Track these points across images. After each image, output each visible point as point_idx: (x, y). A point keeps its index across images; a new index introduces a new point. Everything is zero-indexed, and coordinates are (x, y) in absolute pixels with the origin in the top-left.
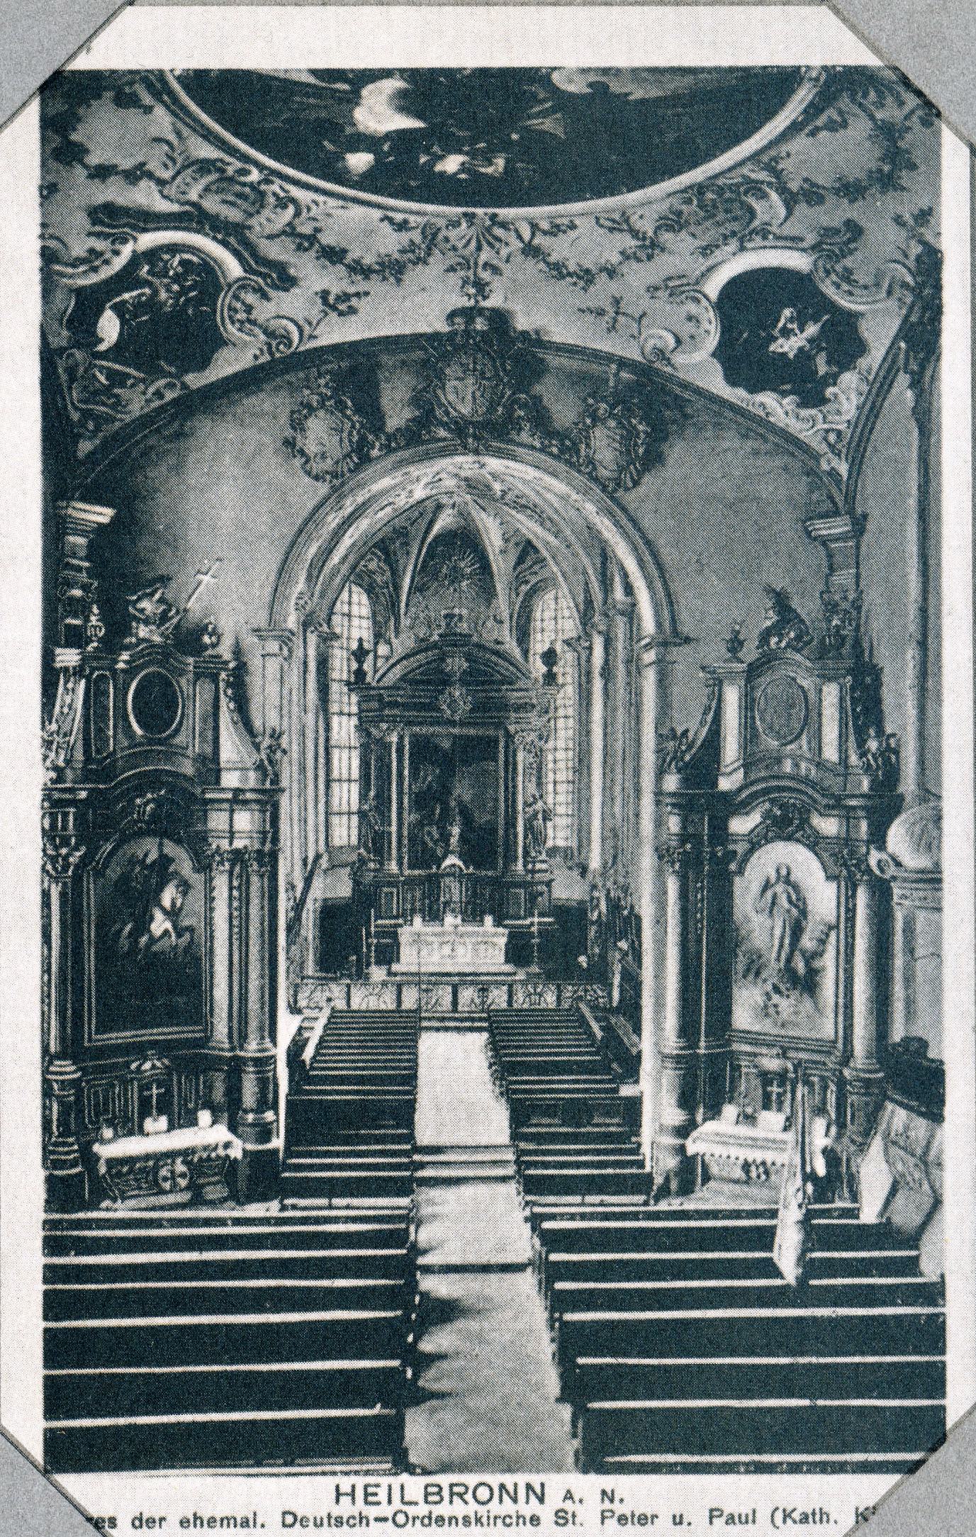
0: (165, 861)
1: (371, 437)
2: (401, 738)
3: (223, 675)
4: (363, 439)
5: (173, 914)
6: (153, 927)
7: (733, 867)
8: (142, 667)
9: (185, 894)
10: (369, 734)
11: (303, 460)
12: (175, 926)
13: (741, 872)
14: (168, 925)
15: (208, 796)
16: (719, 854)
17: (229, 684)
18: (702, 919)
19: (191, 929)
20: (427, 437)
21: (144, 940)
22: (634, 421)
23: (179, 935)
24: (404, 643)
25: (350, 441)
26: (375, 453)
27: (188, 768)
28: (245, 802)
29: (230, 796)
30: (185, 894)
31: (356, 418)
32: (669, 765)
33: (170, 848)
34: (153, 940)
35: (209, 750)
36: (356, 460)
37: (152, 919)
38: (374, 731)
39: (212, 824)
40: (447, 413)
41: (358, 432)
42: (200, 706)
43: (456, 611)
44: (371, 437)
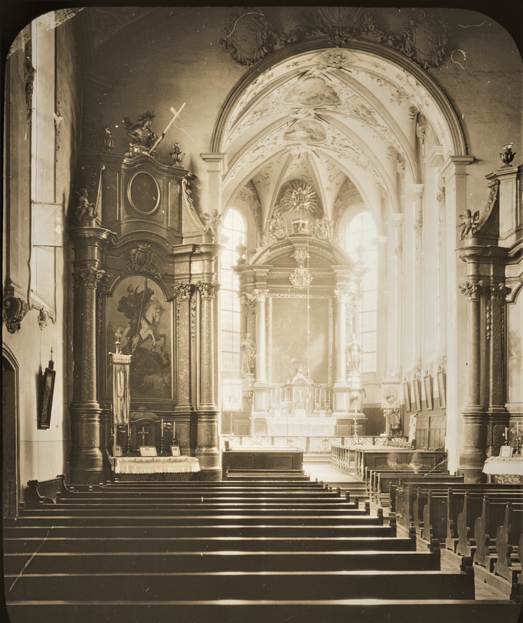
0: (149, 293)
1: (275, 36)
2: (267, 300)
3: (184, 180)
4: (270, 38)
5: (153, 325)
6: (142, 332)
7: (509, 298)
8: (136, 170)
9: (161, 314)
10: (246, 299)
11: (233, 50)
12: (154, 333)
13: (513, 301)
14: (151, 332)
15: (176, 252)
16: (501, 288)
17: (188, 187)
18: (490, 329)
19: (164, 336)
20: (310, 37)
21: (136, 340)
22: (441, 22)
23: (157, 340)
24: (269, 241)
25: (262, 39)
26: (277, 47)
27: (164, 234)
28: (201, 254)
29: (190, 250)
30: (161, 314)
31: (265, 23)
32: (467, 233)
33: (154, 286)
34: (141, 341)
35: (176, 225)
36: (266, 51)
37: (140, 327)
38: (249, 296)
39: (177, 272)
40: (322, 22)
41: (267, 33)
42: (171, 200)
43: (301, 221)
44: (275, 36)
